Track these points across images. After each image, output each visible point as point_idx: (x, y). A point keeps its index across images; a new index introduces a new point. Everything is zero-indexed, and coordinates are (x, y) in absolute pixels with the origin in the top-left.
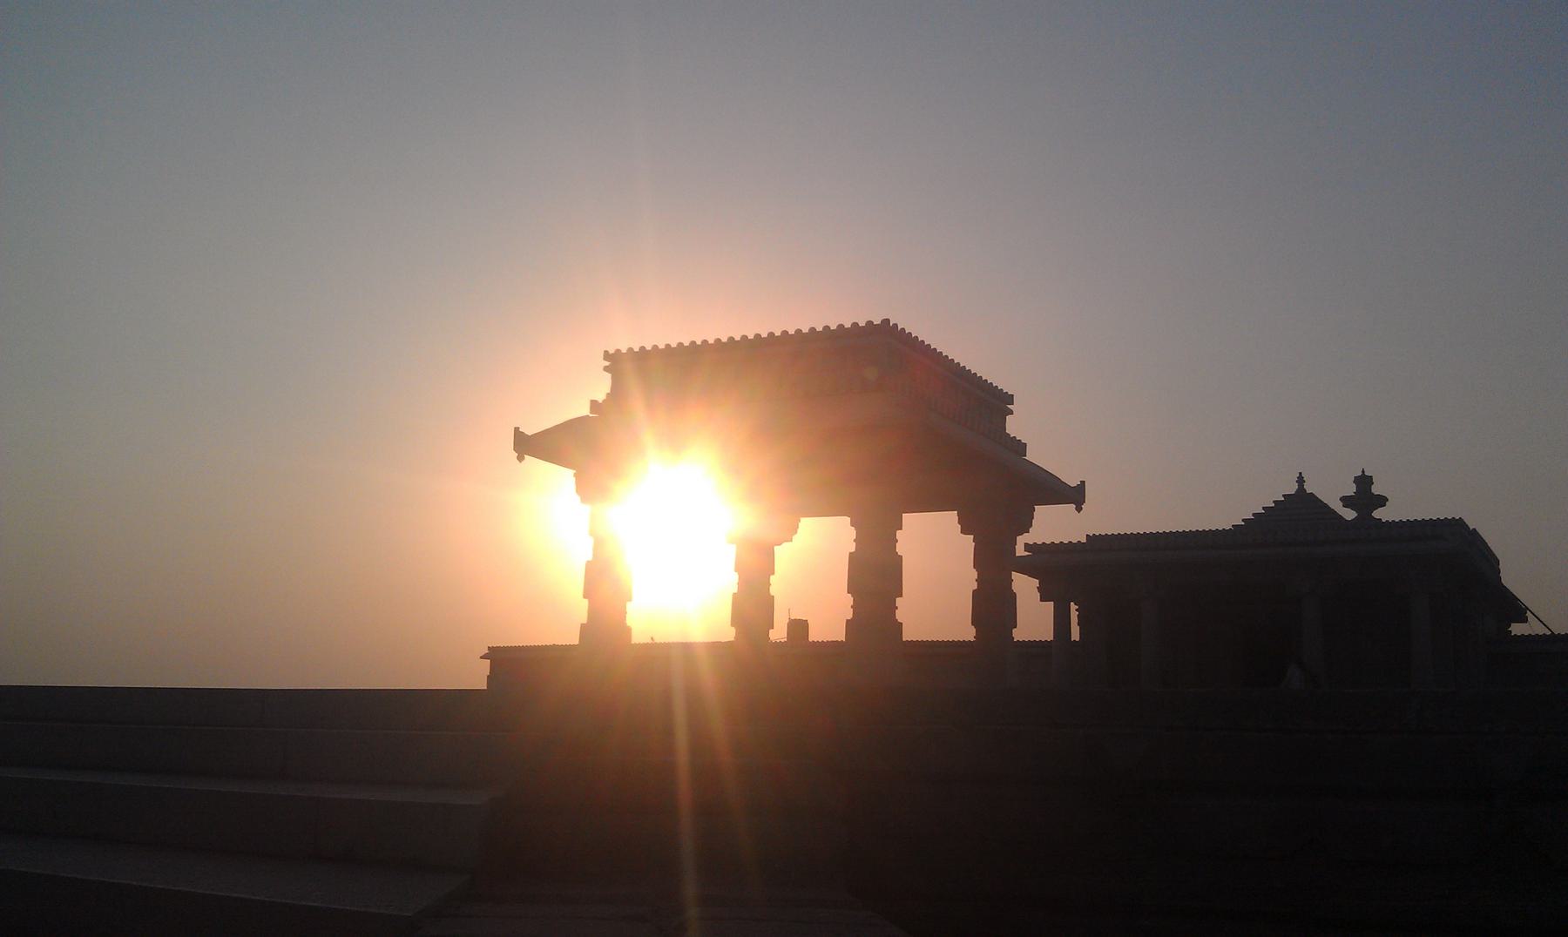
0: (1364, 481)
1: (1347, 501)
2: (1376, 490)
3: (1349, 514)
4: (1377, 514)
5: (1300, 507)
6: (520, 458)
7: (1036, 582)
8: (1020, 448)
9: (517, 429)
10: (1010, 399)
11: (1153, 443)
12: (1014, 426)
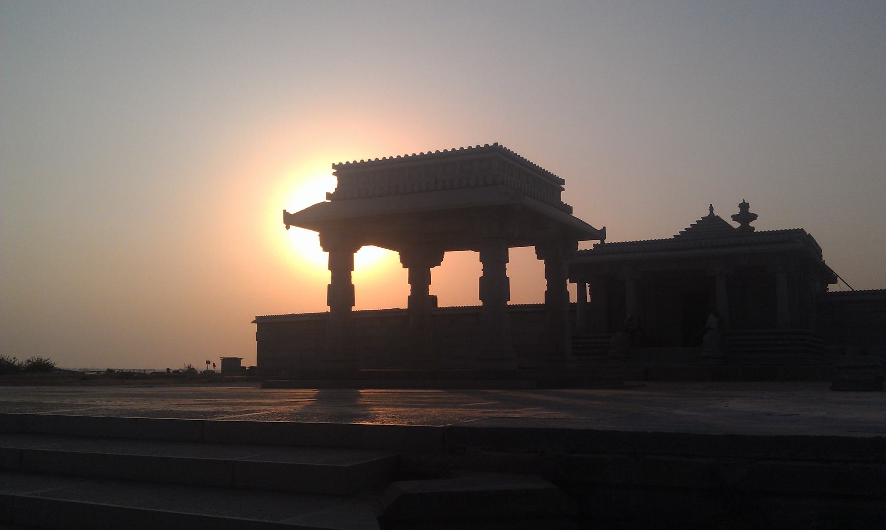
0: (744, 206)
1: (735, 218)
2: (751, 211)
3: (736, 225)
4: (751, 224)
5: (711, 224)
6: (288, 228)
7: (532, 249)
8: (569, 209)
9: (285, 211)
10: (562, 182)
11: (630, 190)
12: (566, 198)
